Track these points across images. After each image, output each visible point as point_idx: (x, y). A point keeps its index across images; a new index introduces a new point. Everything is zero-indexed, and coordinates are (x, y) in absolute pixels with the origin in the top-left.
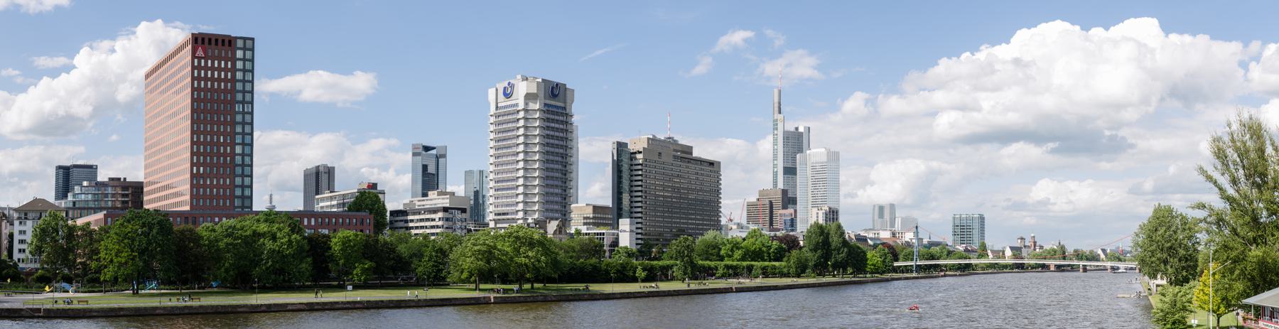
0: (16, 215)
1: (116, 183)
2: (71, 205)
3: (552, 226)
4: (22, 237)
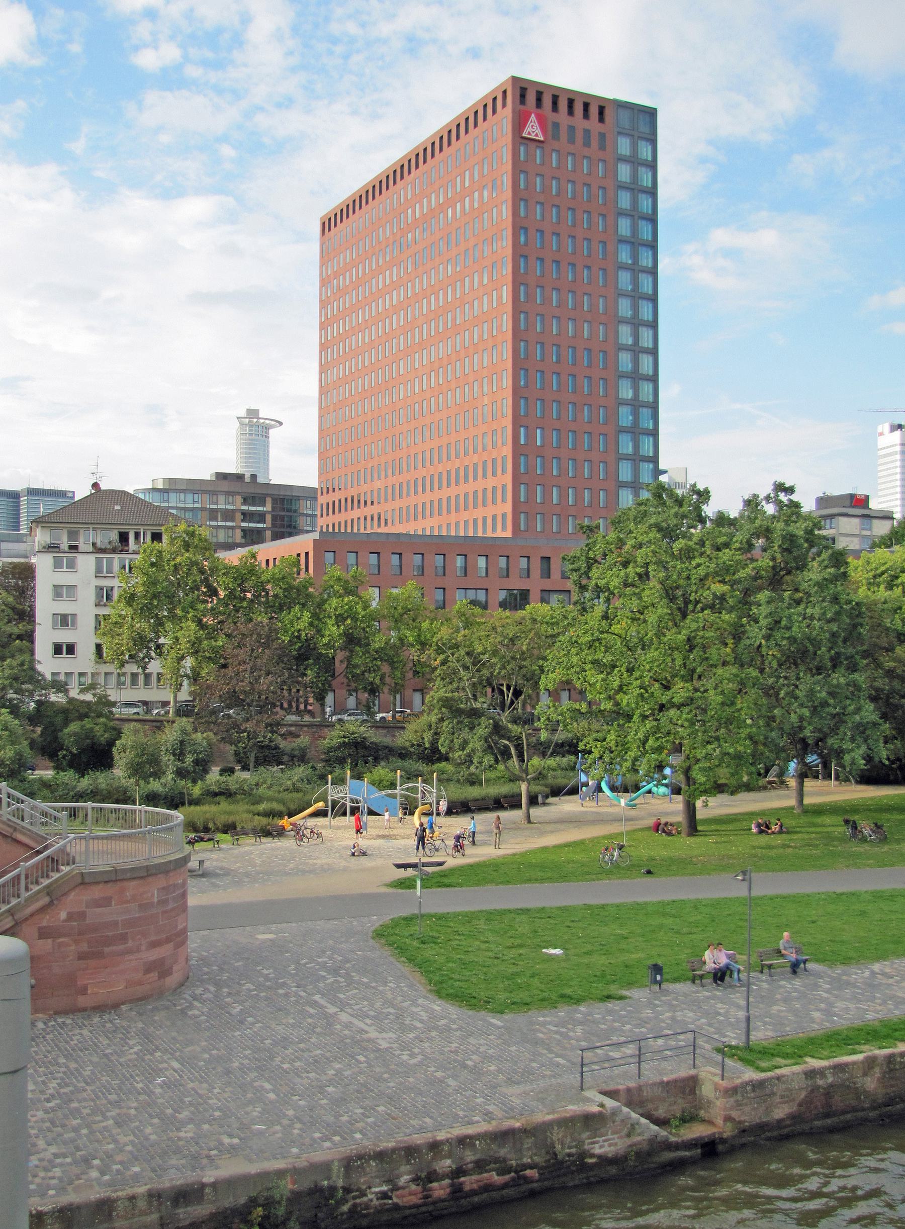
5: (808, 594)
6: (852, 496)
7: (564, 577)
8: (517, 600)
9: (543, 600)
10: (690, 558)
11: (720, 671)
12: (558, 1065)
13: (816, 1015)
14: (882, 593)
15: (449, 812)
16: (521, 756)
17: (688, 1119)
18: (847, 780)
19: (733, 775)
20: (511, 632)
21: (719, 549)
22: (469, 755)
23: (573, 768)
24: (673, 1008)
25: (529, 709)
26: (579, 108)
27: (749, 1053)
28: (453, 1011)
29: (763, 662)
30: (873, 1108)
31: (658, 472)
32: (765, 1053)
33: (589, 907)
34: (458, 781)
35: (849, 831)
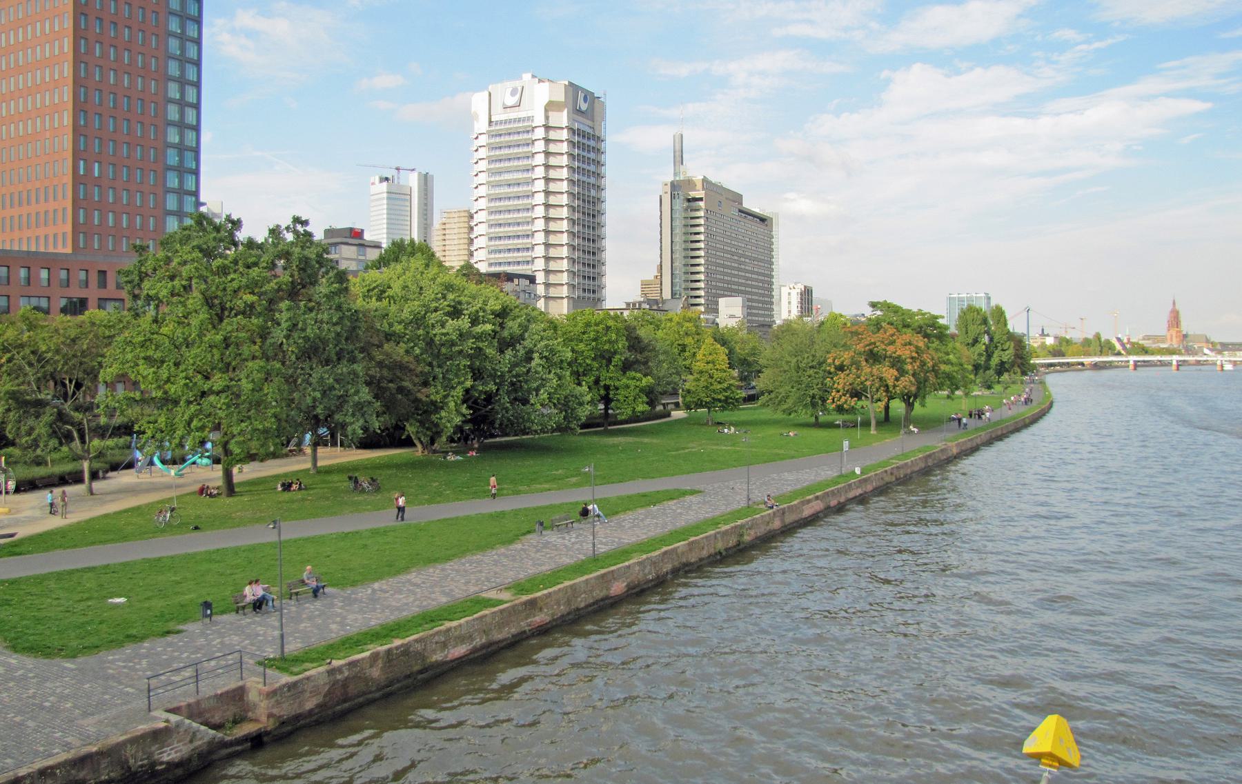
5: (319, 304)
6: (351, 229)
7: (119, 287)
8: (77, 307)
9: (99, 307)
10: (226, 274)
11: (250, 364)
12: (128, 694)
13: (334, 627)
14: (374, 304)
15: (17, 490)
16: (83, 441)
17: (236, 722)
18: (349, 446)
19: (262, 446)
20: (73, 333)
21: (249, 267)
22: (35, 440)
23: (129, 447)
24: (222, 635)
25: (88, 399)
27: (284, 662)
28: (29, 661)
29: (284, 357)
30: (378, 690)
31: (199, 204)
32: (296, 660)
33: (148, 561)
34: (25, 463)
35: (352, 485)
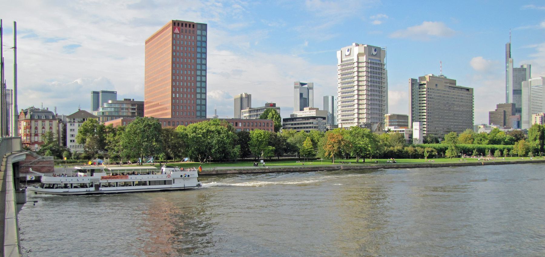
0: (68, 120)
1: (128, 102)
2: (101, 114)
3: (375, 127)
4: (72, 133)
26: (188, 26)
